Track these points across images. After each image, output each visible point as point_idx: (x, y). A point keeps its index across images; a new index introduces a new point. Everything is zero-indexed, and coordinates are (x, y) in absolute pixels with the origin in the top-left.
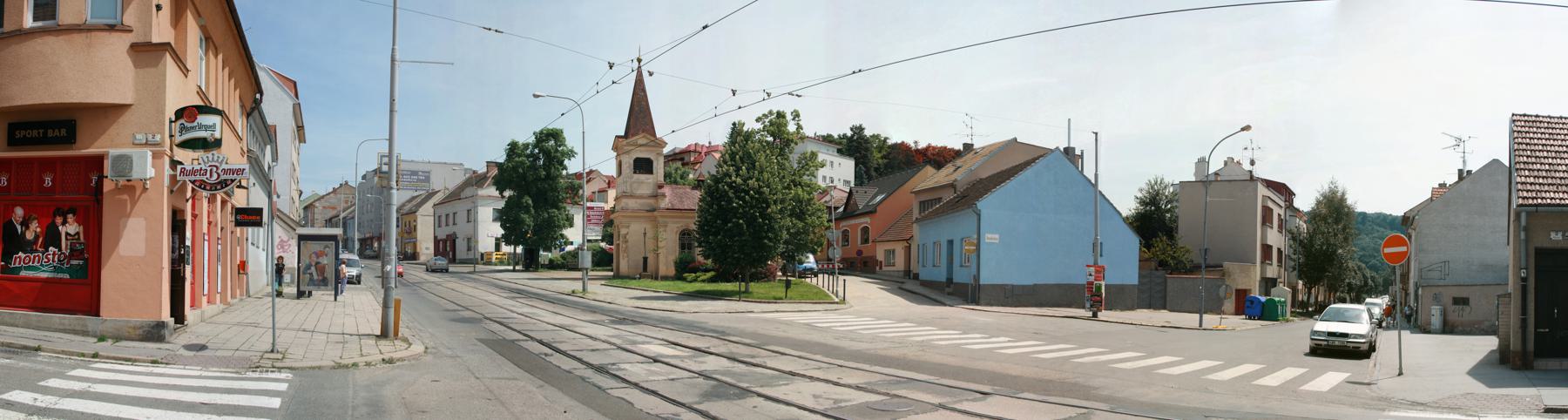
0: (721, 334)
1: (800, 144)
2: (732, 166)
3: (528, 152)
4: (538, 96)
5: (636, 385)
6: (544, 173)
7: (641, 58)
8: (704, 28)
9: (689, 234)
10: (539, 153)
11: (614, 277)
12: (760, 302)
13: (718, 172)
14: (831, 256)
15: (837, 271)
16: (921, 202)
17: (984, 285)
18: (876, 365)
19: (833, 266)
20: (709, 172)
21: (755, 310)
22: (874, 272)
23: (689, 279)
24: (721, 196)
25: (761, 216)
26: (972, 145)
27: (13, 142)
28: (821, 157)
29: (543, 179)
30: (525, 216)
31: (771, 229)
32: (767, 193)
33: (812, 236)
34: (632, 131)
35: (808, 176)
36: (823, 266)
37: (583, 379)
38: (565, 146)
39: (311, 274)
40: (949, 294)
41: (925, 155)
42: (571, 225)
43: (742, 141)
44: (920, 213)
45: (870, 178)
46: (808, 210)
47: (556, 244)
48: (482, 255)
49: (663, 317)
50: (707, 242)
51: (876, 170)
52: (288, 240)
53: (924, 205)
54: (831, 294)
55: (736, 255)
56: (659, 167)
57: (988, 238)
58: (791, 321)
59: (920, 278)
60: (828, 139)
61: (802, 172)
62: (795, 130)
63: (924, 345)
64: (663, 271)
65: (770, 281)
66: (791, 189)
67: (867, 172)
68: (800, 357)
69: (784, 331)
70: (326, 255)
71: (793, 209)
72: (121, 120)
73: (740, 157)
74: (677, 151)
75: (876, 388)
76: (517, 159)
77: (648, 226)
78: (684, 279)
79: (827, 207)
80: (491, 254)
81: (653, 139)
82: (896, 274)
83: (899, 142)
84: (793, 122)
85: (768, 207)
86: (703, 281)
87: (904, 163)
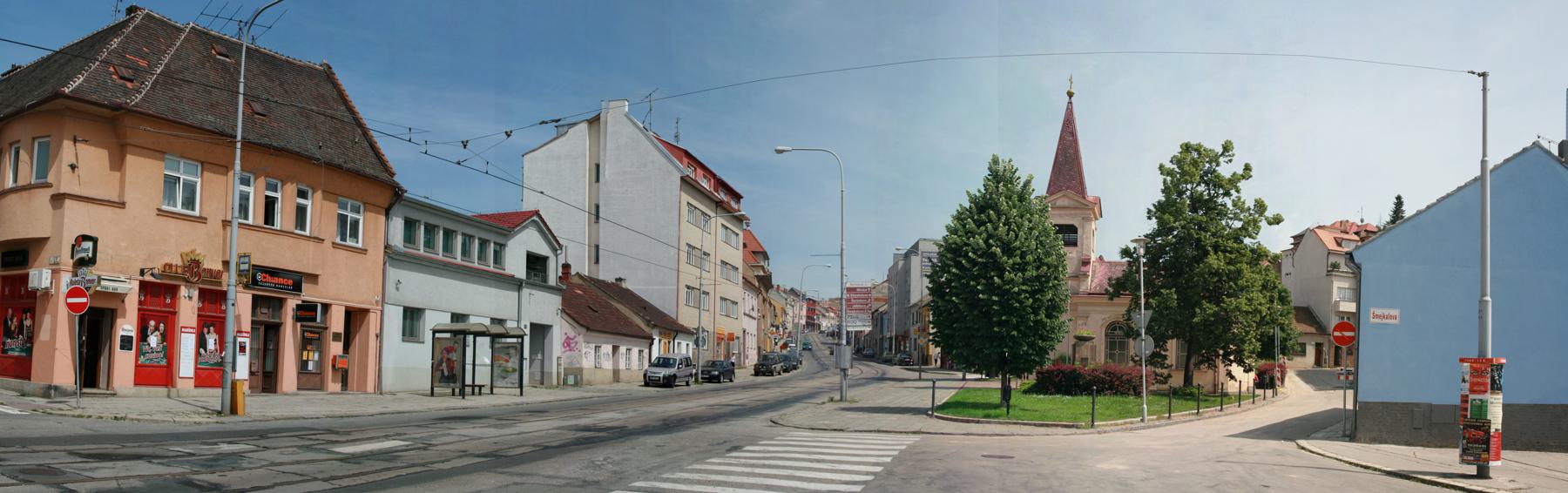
7: (1073, 90)
27: (6, 266)
39: (442, 370)
52: (575, 337)
70: (455, 351)
72: (45, 248)
81: (1082, 201)
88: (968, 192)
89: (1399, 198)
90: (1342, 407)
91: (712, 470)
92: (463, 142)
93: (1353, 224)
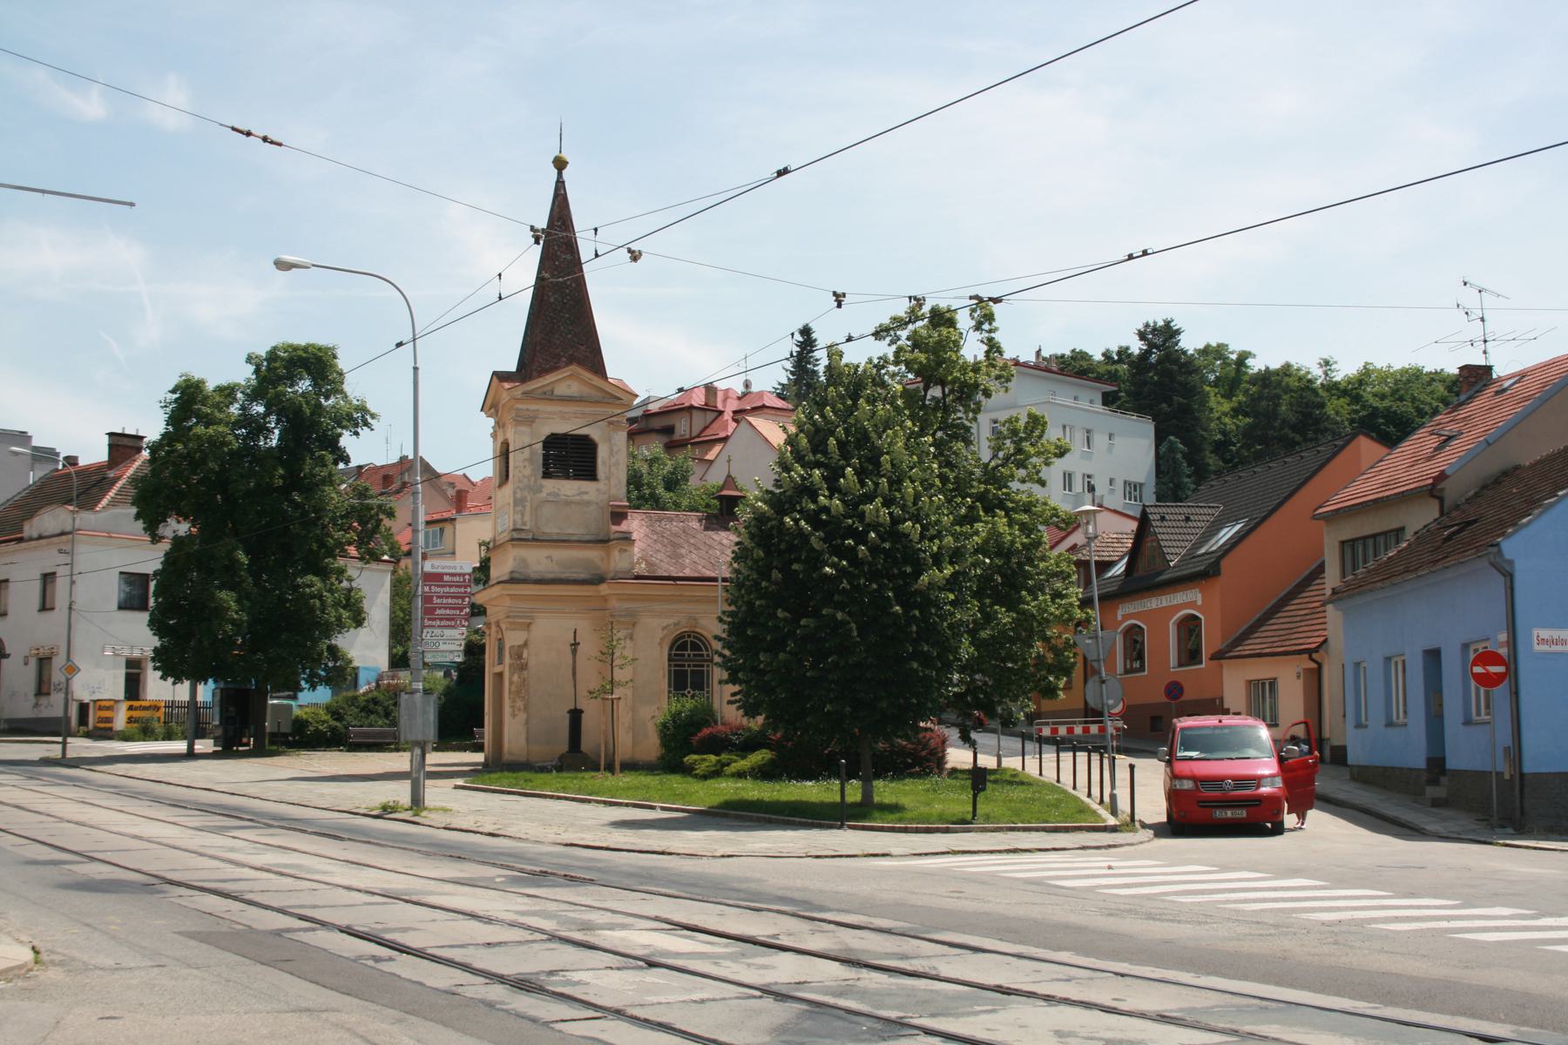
0: (805, 909)
1: (998, 397)
2: (818, 465)
3: (234, 410)
5: (618, 1013)
7: (566, 155)
8: (780, 173)
9: (695, 647)
10: (267, 414)
11: (488, 767)
13: (777, 483)
14: (1092, 703)
17: (1535, 775)
18: (1209, 974)
19: (1102, 730)
21: (894, 851)
23: (701, 768)
24: (791, 548)
26: (1488, 369)
30: (227, 597)
31: (929, 632)
32: (915, 537)
35: (1023, 481)
37: (490, 1005)
40: (1437, 803)
42: (359, 620)
43: (842, 397)
44: (1343, 575)
45: (1201, 474)
48: (83, 708)
50: (754, 669)
54: (1095, 806)
56: (614, 455)
57: (1543, 641)
58: (993, 875)
59: (1351, 760)
60: (1073, 367)
62: (981, 357)
63: (1338, 933)
64: (625, 747)
67: (1193, 457)
68: (1020, 956)
71: (985, 580)
74: (654, 407)
75: (1205, 1019)
76: (200, 429)
78: (687, 771)
79: (1079, 563)
80: (111, 706)
81: (597, 381)
83: (1275, 365)
84: (978, 336)
85: (917, 573)
86: (740, 775)
87: (1294, 428)
91: (1503, 927)
92: (835, 294)
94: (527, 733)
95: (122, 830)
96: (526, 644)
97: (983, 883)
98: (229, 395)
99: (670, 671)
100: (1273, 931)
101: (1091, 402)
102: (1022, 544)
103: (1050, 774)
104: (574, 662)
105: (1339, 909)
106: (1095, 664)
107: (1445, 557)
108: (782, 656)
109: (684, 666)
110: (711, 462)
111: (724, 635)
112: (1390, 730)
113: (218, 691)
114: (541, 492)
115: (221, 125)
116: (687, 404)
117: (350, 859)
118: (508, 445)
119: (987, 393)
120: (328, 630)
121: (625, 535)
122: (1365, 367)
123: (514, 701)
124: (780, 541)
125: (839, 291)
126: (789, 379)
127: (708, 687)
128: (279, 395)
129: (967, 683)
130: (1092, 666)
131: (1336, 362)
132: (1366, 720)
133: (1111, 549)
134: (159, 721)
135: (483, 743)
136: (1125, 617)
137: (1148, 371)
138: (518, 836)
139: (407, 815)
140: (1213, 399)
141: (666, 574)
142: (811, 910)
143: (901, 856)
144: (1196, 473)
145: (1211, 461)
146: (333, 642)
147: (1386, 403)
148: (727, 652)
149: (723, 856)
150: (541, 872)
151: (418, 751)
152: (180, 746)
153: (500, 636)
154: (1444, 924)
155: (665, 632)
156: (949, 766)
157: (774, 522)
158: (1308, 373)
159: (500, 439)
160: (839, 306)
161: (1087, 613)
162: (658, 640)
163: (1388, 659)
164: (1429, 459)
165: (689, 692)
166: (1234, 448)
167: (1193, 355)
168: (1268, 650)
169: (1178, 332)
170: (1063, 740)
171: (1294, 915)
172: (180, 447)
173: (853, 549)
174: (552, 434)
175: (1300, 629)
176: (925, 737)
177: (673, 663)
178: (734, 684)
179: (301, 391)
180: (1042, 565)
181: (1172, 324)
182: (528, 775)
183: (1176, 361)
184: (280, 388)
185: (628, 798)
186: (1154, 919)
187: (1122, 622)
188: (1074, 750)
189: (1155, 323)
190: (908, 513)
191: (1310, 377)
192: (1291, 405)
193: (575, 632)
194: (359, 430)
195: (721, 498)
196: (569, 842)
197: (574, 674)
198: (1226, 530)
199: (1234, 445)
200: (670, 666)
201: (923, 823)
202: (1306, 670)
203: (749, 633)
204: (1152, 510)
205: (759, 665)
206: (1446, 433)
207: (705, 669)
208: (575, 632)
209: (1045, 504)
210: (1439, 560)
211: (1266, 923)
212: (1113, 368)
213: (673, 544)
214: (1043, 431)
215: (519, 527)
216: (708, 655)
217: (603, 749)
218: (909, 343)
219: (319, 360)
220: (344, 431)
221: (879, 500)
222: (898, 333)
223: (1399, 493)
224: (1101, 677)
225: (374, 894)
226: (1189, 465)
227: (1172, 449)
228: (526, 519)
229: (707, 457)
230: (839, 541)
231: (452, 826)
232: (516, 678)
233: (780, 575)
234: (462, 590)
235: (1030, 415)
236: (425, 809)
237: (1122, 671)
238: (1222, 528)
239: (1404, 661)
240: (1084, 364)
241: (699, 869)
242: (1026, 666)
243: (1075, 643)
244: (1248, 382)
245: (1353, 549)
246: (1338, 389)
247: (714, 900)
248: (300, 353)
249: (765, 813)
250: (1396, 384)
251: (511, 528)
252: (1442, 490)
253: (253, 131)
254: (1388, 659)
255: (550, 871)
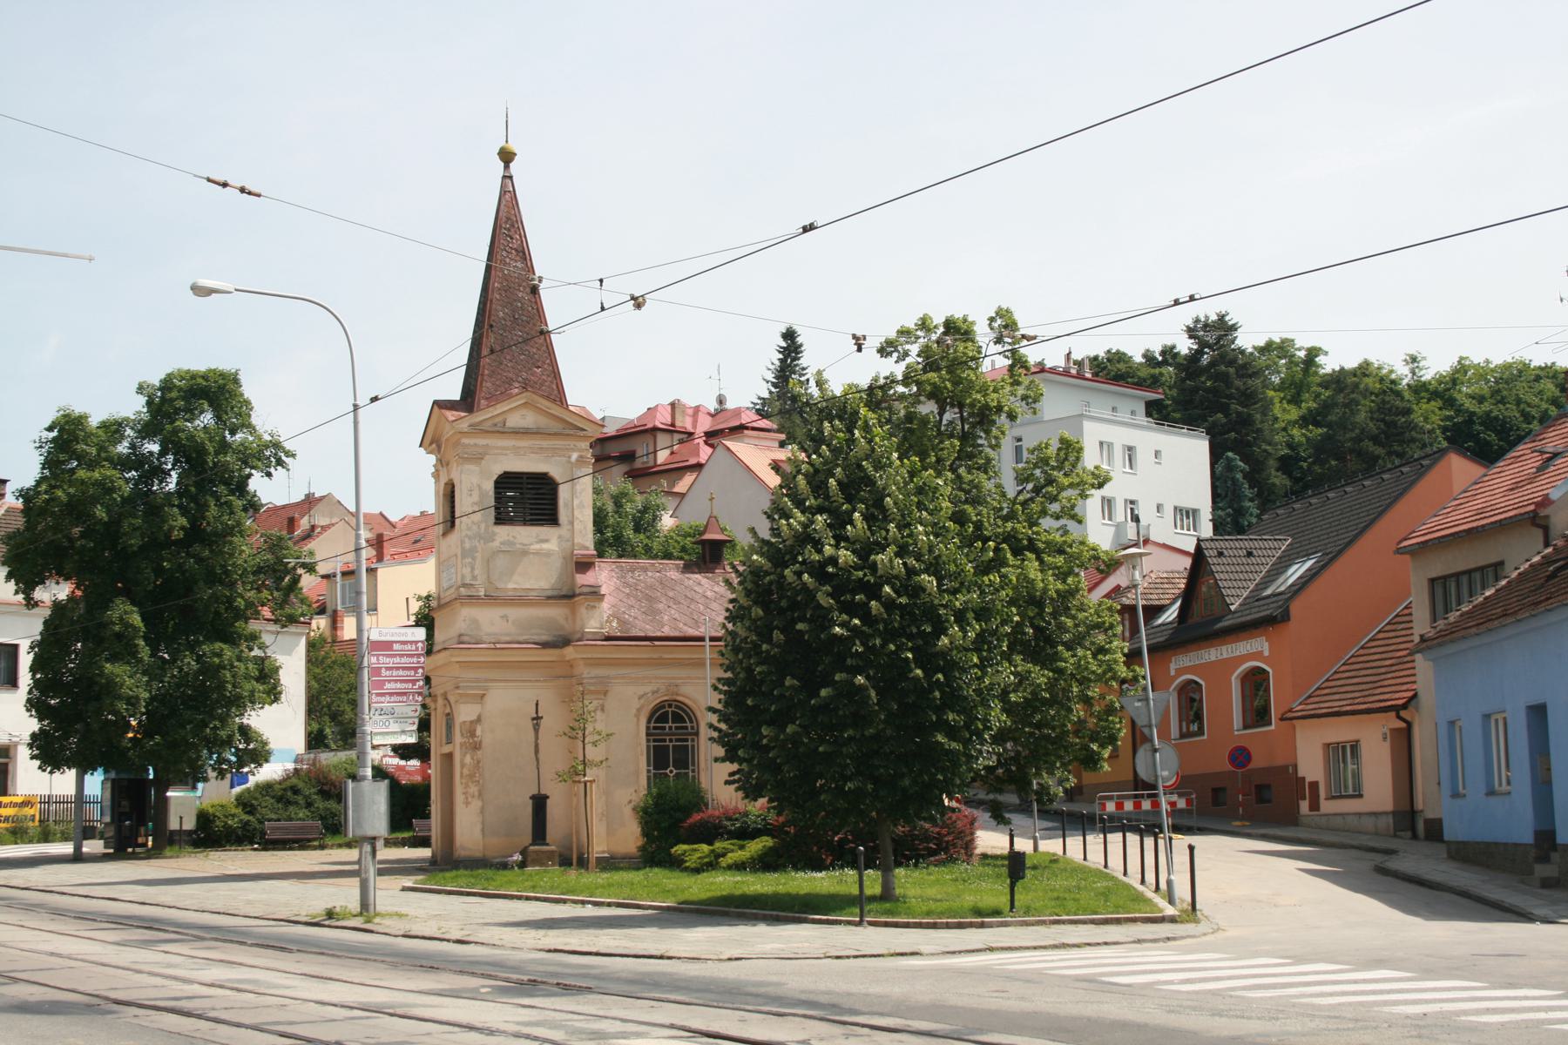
2: (820, 510)
4: (209, 292)
6: (183, 521)
8: (806, 229)
9: (678, 718)
10: (163, 453)
12: (934, 926)
13: (775, 531)
14: (1143, 773)
15: (1166, 822)
16: (1432, 581)
19: (1156, 805)
20: (753, 531)
21: (924, 949)
22: (1292, 819)
23: (691, 861)
24: (794, 605)
25: (919, 662)
28: (1092, 436)
29: (178, 542)
31: (953, 699)
33: (1079, 710)
34: (487, 385)
36: (1120, 806)
38: (251, 428)
40: (1546, 884)
41: (1450, 402)
42: (274, 695)
44: (1434, 620)
45: (1266, 498)
46: (1062, 628)
47: (221, 761)
49: (649, 974)
50: (756, 746)
51: (1286, 464)
53: (1443, 590)
54: (1150, 894)
55: (849, 785)
58: (1039, 972)
61: (1035, 507)
65: (952, 860)
66: (1004, 563)
67: (1255, 475)
69: (1022, 999)
73: (839, 483)
76: (82, 474)
77: (547, 696)
78: (676, 864)
81: (556, 410)
82: (1368, 823)
83: (1351, 363)
85: (941, 630)
86: (739, 867)
87: (1375, 439)
88: (791, 346)
89: (789, 335)
90: (1109, 836)
92: (854, 337)
93: (697, 409)
94: (483, 823)
95: (33, 947)
96: (479, 720)
97: (1028, 981)
98: (117, 431)
99: (648, 747)
100: (1351, 1026)
101: (1133, 413)
102: (1057, 591)
103: (1095, 857)
104: (537, 738)
105: (1427, 1001)
106: (1146, 731)
107: (1547, 599)
108: (790, 729)
109: (665, 741)
110: (682, 496)
111: (720, 707)
112: (1493, 800)
113: (109, 785)
114: (493, 540)
115: (195, 176)
116: (650, 426)
117: (308, 973)
118: (453, 486)
119: (1012, 417)
120: (239, 703)
121: (593, 590)
122: (1459, 362)
123: (467, 786)
124: (780, 598)
125: (859, 334)
126: (771, 392)
127: (693, 764)
128: (176, 431)
129: (999, 755)
130: (1142, 733)
131: (1424, 358)
132: (1464, 788)
133: (1161, 591)
134: (33, 820)
135: (430, 836)
136: (1180, 672)
137: (1200, 375)
138: (491, 942)
139: (357, 922)
140: (1278, 405)
141: (643, 634)
142: (841, 1014)
143: (932, 954)
144: (1259, 495)
145: (1277, 481)
146: (245, 721)
147: (1486, 407)
148: (723, 726)
149: (730, 959)
150: (529, 980)
151: (367, 848)
152: (67, 848)
153: (448, 710)
154: (1542, 1015)
155: (642, 701)
156: (978, 851)
157: (772, 577)
158: (1391, 372)
159: (443, 480)
160: (859, 350)
161: (1134, 671)
162: (634, 711)
163: (1487, 717)
164: (1531, 480)
165: (671, 772)
166: (1305, 465)
167: (1251, 354)
168: (1348, 708)
169: (1234, 328)
170: (1112, 818)
171: (1376, 1009)
172: (59, 493)
173: (866, 605)
174: (505, 473)
175: (1386, 683)
176: (950, 818)
177: (652, 738)
178: (732, 762)
179: (202, 425)
180: (1081, 616)
181: (1227, 318)
182: (490, 873)
183: (1232, 362)
184: (178, 423)
185: (609, 897)
186: (1221, 1016)
187: (1175, 678)
188: (1124, 829)
189: (1207, 317)
190: (923, 562)
191: (1393, 376)
192: (1371, 412)
193: (537, 705)
194: (272, 470)
195: (703, 543)
196: (552, 948)
197: (537, 751)
198: (1296, 567)
199: (1305, 461)
200: (648, 741)
201: (954, 917)
202: (1393, 730)
203: (749, 702)
204: (1208, 544)
205: (761, 740)
206: (1551, 450)
207: (689, 743)
208: (537, 705)
209: (1082, 543)
210: (1541, 602)
211: (1344, 1018)
212: (1157, 371)
213: (650, 599)
214: (1078, 459)
215: (468, 582)
216: (692, 728)
217: (574, 840)
218: (920, 360)
219: (222, 388)
220: (253, 471)
221: (891, 550)
222: (907, 347)
223: (1496, 522)
224: (1153, 745)
225: (352, 1008)
226: (1251, 487)
227: (1230, 467)
228: (476, 572)
229: (676, 490)
230: (848, 597)
231: (412, 933)
232: (468, 759)
233: (782, 637)
234: (415, 660)
235: (1063, 440)
236: (377, 915)
237: (1178, 736)
238: (1290, 565)
239: (1505, 719)
240: (1121, 366)
241: (708, 974)
242: (1065, 733)
243: (1122, 707)
244: (1320, 385)
245: (1445, 588)
246: (1427, 390)
247: (731, 1006)
248: (200, 381)
249: (773, 910)
250: (1496, 382)
251: (459, 583)
252: (1547, 517)
253: (229, 182)
254: (1487, 717)
255: (539, 979)
